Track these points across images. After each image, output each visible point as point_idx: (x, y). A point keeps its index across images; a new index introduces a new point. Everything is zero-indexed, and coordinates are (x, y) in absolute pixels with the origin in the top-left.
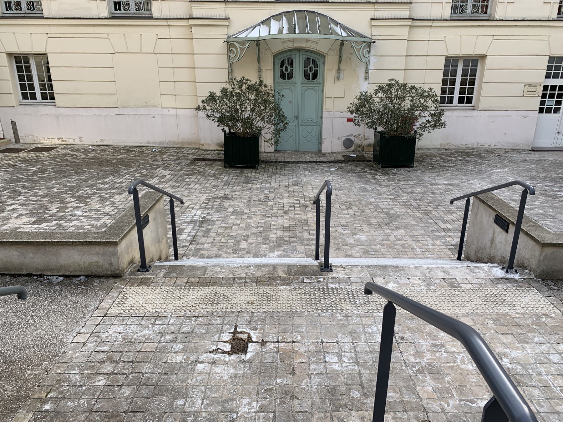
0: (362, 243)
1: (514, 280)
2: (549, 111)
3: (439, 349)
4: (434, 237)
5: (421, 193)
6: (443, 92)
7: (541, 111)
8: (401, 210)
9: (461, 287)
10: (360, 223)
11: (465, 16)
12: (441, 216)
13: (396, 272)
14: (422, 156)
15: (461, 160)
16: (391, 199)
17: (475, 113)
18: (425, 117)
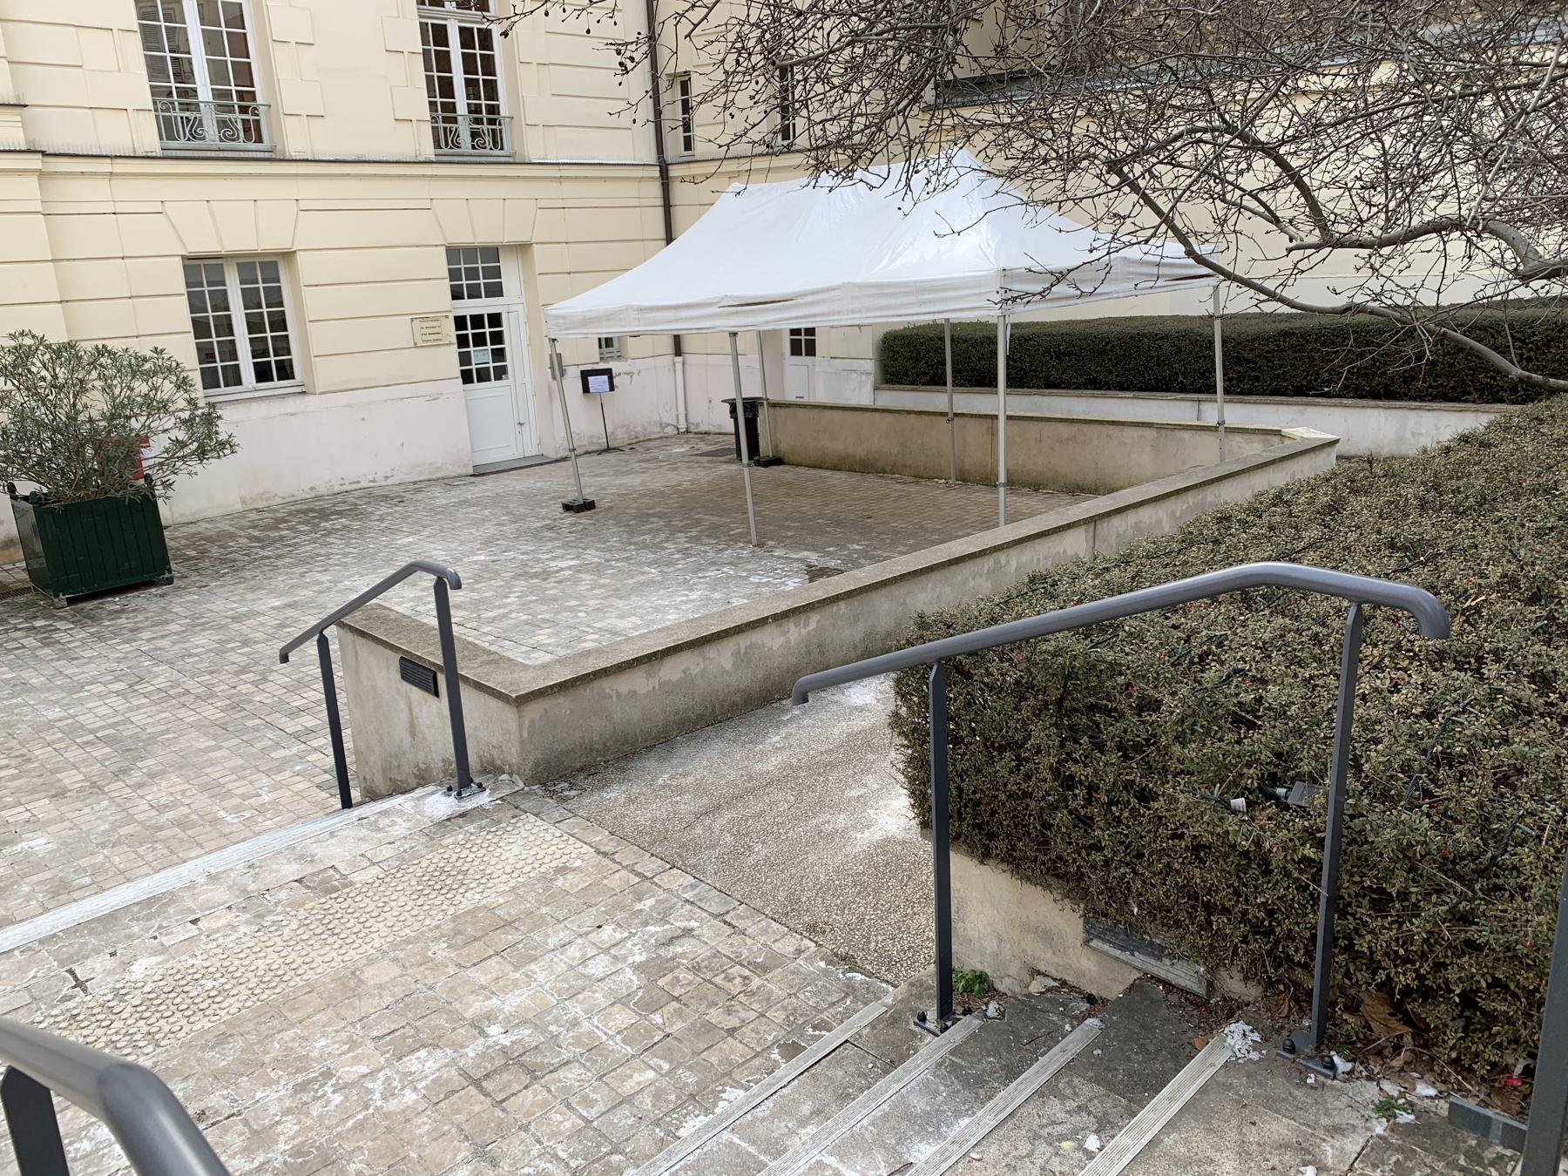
0: (39, 865)
1: (480, 811)
2: (483, 376)
3: (316, 1091)
4: (270, 765)
5: (211, 651)
6: (205, 354)
7: (467, 377)
8: (157, 717)
9: (352, 884)
10: (23, 800)
11: (204, 147)
12: (281, 701)
13: (149, 918)
14: (194, 543)
15: (306, 533)
16: (118, 693)
17: (310, 402)
18: (165, 431)
